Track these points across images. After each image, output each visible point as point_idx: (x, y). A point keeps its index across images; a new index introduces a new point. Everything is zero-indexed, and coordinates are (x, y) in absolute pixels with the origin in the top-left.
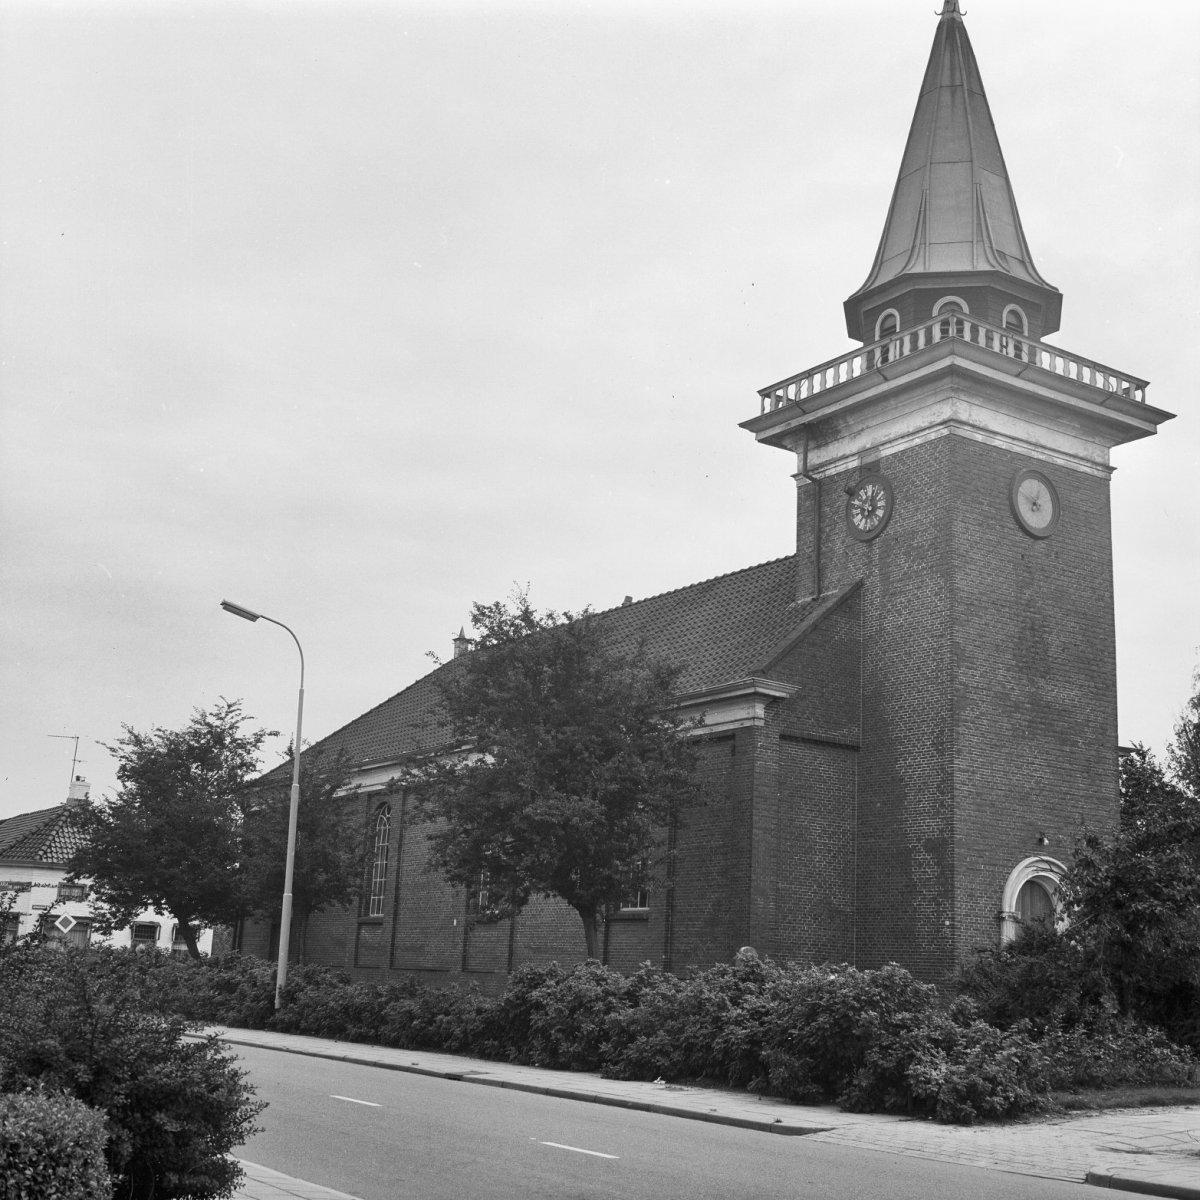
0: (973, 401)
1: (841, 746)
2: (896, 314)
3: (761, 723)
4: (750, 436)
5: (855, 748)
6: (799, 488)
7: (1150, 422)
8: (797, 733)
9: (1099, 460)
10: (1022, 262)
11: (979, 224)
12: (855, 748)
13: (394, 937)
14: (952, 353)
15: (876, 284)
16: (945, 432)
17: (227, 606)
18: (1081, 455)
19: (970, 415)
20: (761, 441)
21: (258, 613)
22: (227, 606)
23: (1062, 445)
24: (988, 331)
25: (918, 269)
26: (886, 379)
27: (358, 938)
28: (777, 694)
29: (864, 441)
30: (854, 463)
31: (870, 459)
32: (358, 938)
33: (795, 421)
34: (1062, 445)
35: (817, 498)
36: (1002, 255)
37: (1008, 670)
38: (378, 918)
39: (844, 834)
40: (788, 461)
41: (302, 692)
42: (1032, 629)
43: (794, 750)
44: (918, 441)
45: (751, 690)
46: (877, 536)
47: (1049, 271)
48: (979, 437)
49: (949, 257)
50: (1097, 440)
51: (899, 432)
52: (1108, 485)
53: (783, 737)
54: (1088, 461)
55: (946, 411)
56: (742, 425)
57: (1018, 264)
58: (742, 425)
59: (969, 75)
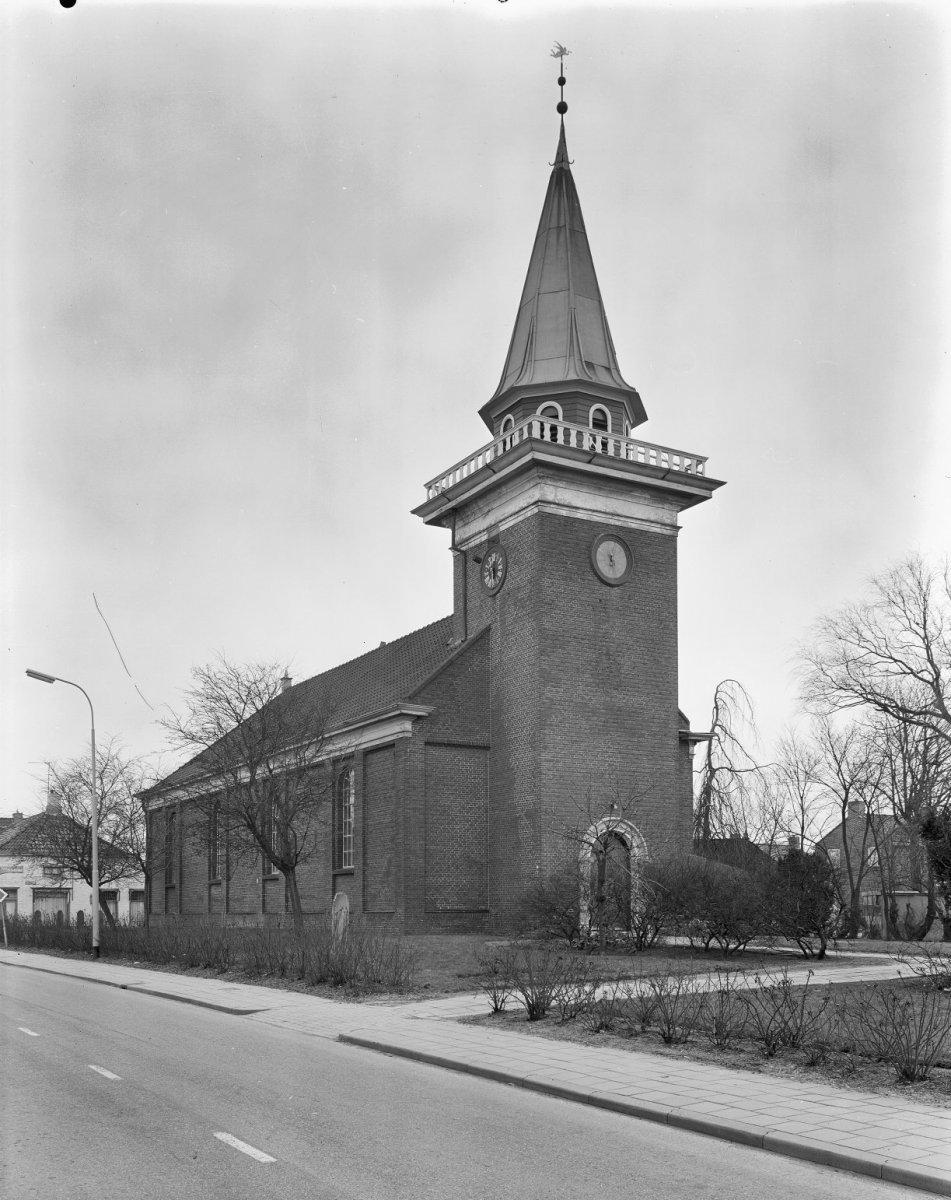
0: (559, 484)
1: (480, 747)
2: (512, 419)
3: (410, 735)
4: (419, 520)
5: (486, 748)
6: (455, 557)
7: (707, 489)
8: (439, 740)
9: (668, 521)
10: (608, 369)
11: (572, 341)
12: (486, 748)
13: (228, 894)
14: (532, 450)
15: (504, 391)
16: (536, 510)
17: (30, 673)
18: (652, 518)
19: (556, 496)
20: (426, 523)
21: (55, 676)
22: (30, 673)
23: (637, 512)
24: (565, 429)
25: (524, 382)
26: (495, 472)
27: (210, 895)
28: (419, 713)
29: (490, 520)
30: (484, 537)
31: (494, 533)
32: (210, 895)
33: (447, 509)
34: (637, 512)
35: (466, 559)
36: (590, 365)
37: (587, 686)
38: (349, 870)
39: (479, 808)
40: (444, 535)
41: (93, 730)
42: (608, 654)
43: (434, 752)
44: (521, 519)
45: (398, 712)
46: (498, 592)
47: (632, 372)
48: (564, 512)
49: (551, 369)
50: (666, 506)
51: (512, 509)
52: (676, 541)
53: (427, 743)
54: (658, 523)
55: (536, 494)
56: (413, 512)
57: (604, 371)
58: (413, 512)
59: (572, 217)
